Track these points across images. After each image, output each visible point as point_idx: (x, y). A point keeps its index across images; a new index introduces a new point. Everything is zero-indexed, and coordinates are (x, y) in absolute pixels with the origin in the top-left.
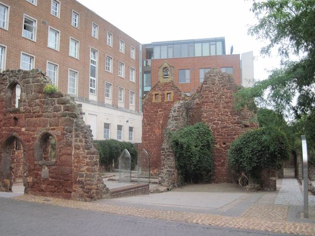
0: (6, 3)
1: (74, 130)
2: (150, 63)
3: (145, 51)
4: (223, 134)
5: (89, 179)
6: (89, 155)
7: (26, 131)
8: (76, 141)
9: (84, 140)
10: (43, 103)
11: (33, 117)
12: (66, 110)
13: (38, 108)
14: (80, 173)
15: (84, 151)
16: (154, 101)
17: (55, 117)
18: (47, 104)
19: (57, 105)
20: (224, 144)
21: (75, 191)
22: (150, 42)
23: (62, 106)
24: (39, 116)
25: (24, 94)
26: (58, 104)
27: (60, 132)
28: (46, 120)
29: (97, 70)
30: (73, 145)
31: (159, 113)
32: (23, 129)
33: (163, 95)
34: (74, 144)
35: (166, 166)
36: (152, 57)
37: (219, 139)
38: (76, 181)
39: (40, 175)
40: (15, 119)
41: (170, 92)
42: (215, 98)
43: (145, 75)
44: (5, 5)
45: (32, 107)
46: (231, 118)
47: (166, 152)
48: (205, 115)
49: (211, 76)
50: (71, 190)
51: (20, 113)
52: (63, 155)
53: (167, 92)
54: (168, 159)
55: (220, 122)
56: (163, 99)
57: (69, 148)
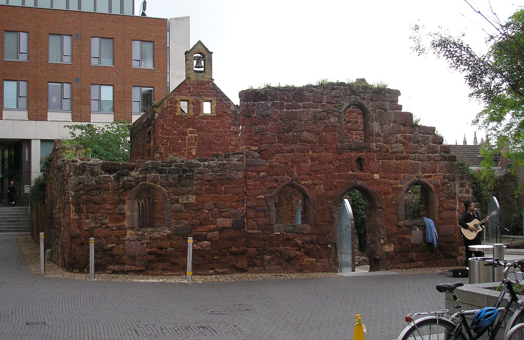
2: (95, 51)
8: (461, 192)
13: (400, 147)
28: (416, 163)
32: (376, 176)
40: (359, 160)
57: (452, 201)
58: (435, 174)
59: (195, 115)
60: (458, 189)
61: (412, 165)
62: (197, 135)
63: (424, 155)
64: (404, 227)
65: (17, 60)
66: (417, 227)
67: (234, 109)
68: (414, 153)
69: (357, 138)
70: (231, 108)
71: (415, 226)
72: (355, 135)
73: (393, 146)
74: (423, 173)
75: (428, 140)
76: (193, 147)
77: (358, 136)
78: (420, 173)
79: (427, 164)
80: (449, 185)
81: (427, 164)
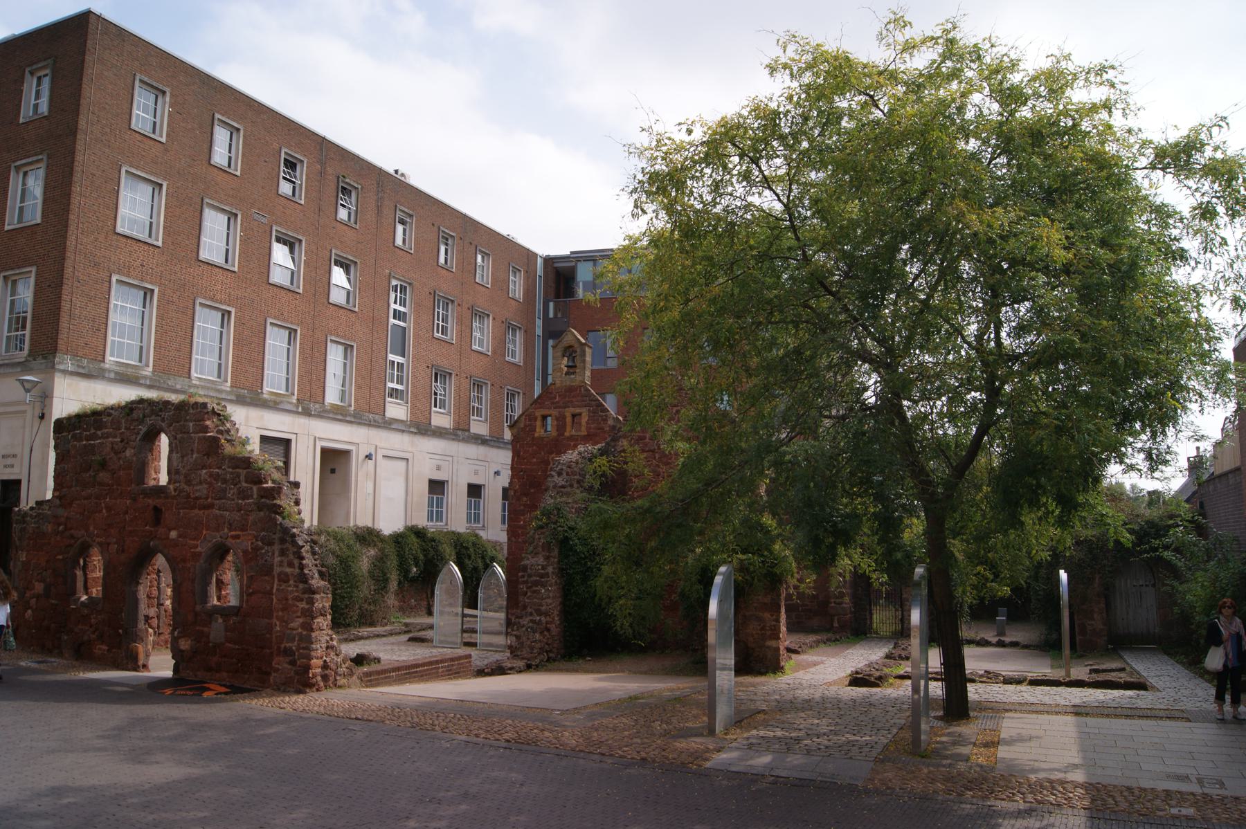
6: (306, 596)
9: (296, 562)
10: (216, 477)
11: (193, 508)
12: (262, 497)
13: (203, 490)
16: (539, 432)
17: (239, 510)
19: (245, 485)
21: (277, 670)
22: (566, 252)
23: (255, 488)
25: (174, 455)
26: (246, 482)
27: (250, 543)
30: (275, 573)
34: (277, 570)
35: (529, 610)
38: (279, 648)
39: (208, 637)
40: (157, 510)
44: (152, 178)
47: (530, 576)
51: (166, 498)
53: (572, 410)
54: (534, 592)
57: (266, 578)
59: (559, 435)
60: (277, 559)
65: (603, 367)
66: (219, 616)
68: (220, 499)
70: (609, 422)
74: (230, 529)
75: (239, 478)
78: (226, 530)
80: (263, 551)
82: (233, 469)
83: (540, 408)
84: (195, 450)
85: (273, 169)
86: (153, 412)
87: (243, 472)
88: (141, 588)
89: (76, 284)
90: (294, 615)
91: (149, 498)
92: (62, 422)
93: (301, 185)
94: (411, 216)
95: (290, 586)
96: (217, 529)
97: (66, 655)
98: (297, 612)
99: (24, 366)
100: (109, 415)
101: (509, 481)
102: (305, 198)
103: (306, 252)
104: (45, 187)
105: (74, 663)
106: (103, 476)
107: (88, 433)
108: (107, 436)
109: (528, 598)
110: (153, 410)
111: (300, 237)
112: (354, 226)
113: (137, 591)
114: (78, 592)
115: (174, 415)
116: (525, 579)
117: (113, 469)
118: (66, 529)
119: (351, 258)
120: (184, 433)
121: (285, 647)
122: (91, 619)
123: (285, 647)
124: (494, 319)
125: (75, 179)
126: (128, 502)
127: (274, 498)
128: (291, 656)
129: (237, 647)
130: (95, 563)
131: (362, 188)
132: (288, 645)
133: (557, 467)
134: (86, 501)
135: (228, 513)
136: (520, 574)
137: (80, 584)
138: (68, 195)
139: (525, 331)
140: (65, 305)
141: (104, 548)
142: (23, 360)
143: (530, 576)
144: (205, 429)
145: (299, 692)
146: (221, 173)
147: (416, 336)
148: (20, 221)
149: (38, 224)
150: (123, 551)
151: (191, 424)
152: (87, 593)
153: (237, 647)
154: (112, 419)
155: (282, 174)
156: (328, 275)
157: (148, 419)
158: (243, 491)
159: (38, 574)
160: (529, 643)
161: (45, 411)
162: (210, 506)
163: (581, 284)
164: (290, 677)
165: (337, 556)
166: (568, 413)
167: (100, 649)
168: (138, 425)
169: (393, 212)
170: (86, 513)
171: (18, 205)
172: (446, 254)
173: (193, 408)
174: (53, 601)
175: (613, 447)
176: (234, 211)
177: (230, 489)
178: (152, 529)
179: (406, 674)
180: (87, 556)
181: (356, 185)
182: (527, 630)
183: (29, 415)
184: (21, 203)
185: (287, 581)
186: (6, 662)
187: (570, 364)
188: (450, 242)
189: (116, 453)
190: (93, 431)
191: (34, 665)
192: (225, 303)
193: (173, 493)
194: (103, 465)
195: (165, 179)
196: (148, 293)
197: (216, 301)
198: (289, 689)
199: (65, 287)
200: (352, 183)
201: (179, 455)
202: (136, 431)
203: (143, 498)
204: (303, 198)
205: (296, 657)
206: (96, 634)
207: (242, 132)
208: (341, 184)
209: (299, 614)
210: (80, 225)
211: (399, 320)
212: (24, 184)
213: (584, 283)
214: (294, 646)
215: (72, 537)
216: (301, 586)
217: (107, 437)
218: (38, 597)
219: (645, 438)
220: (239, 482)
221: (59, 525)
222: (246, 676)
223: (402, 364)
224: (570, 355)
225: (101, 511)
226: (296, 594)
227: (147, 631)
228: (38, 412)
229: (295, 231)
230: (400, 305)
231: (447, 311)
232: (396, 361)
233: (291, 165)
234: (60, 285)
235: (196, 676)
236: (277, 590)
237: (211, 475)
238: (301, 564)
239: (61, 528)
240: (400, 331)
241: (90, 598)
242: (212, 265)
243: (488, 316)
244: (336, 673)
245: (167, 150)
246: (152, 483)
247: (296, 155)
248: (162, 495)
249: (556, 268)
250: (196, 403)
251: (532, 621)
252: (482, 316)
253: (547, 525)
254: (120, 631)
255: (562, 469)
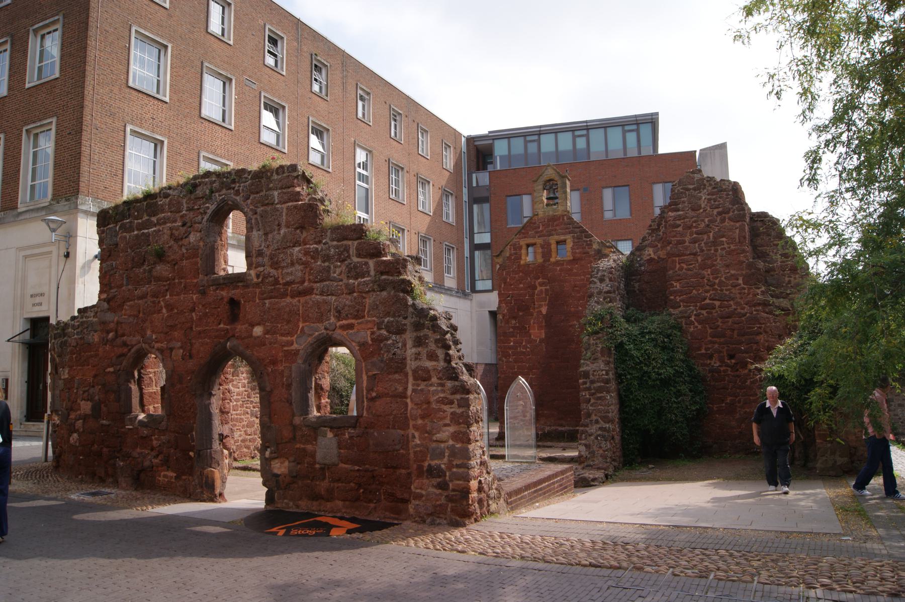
0: (162, 37)
1: (409, 327)
3: (473, 153)
4: (728, 333)
5: (459, 462)
6: (458, 396)
7: (265, 334)
8: (417, 357)
9: (440, 353)
10: (315, 255)
11: (284, 295)
12: (382, 273)
14: (434, 445)
15: (443, 385)
17: (351, 292)
18: (327, 258)
19: (355, 259)
20: (731, 357)
21: (419, 497)
22: (484, 132)
23: (371, 263)
24: (300, 294)
25: (255, 233)
26: (359, 256)
27: (369, 333)
29: (373, 195)
30: (408, 369)
31: (539, 288)
33: (546, 248)
34: (411, 365)
35: (594, 417)
36: (489, 166)
37: (716, 346)
38: (420, 468)
39: (313, 455)
40: (234, 303)
41: (562, 238)
42: (703, 245)
43: (475, 207)
45: (283, 268)
46: (746, 291)
47: (592, 382)
48: (677, 286)
49: (688, 190)
50: (406, 496)
51: (247, 286)
52: (379, 396)
53: (556, 238)
54: (600, 398)
55: (717, 303)
56: (547, 254)
57: (397, 376)
58: (360, 321)
59: (544, 261)
60: (410, 351)
61: (318, 304)
62: (548, 287)
63: (341, 283)
64: (304, 429)
67: (598, 247)
68: (321, 281)
69: (681, 269)
70: (594, 247)
71: (325, 427)
72: (679, 263)
73: (285, 271)
74: (339, 318)
75: (348, 252)
76: (543, 303)
77: (682, 265)
78: (333, 320)
79: (346, 300)
80: (390, 342)
81: (346, 300)
82: (338, 241)
83: (525, 237)
84: (283, 224)
85: (260, 43)
86: (224, 186)
87: (353, 245)
88: (214, 400)
89: (94, 131)
90: (441, 423)
91: (223, 289)
92: (108, 212)
93: (283, 58)
94: (368, 94)
95: (431, 385)
96: (320, 320)
97: (124, 485)
98: (445, 418)
99: (48, 209)
100: (166, 196)
101: (497, 306)
102: (287, 69)
103: (289, 117)
104: (62, 44)
105: (134, 493)
106: (162, 269)
107: (140, 221)
108: (164, 221)
109: (592, 405)
110: (223, 183)
111: (283, 104)
112: (325, 97)
113: (210, 404)
114: (133, 410)
115: (252, 184)
116: (588, 385)
117: (173, 260)
118: (116, 336)
119: (325, 126)
120: (267, 204)
121: (429, 465)
122: (151, 440)
123: (429, 465)
124: (433, 185)
125: (90, 33)
126: (194, 297)
127: (400, 273)
128: (440, 477)
129: (357, 468)
130: (151, 375)
131: (331, 66)
132: (433, 463)
133: (597, 273)
134: (140, 301)
135: (334, 298)
136: (581, 381)
137: (135, 401)
138: (84, 48)
139: (456, 197)
140: (85, 150)
141: (165, 354)
142: (47, 204)
143: (592, 382)
144: (297, 196)
145: (457, 525)
146: (217, 41)
147: (377, 196)
148: (39, 78)
149: (57, 79)
150: (191, 357)
151: (276, 193)
152: (143, 411)
153: (357, 468)
154: (171, 200)
155: (267, 48)
156: (306, 139)
157: (217, 194)
158: (355, 267)
159: (84, 392)
160: (601, 452)
161: (69, 250)
162: (309, 292)
163: (498, 158)
164: (440, 505)
165: (348, 379)
166: (553, 240)
167: (165, 476)
168: (204, 203)
169: (355, 89)
170: (141, 315)
171: (30, 183)
172: (395, 128)
173: (278, 174)
174: (104, 422)
175: (639, 256)
176: (229, 76)
177: (336, 267)
178: (228, 327)
179: (535, 492)
180: (142, 368)
181: (325, 63)
182: (596, 438)
183: (55, 254)
184: (32, 181)
185: (427, 379)
186: (53, 495)
187: (552, 196)
188: (398, 118)
189: (177, 240)
190: (146, 218)
191: (89, 499)
192: (224, 157)
193: (255, 280)
194: (160, 256)
195: (170, 41)
196: (158, 144)
197: (217, 155)
198: (438, 521)
199: (84, 133)
200: (323, 61)
201: (261, 233)
202: (201, 211)
203: (215, 290)
204: (285, 70)
205: (447, 478)
206: (160, 458)
207: (233, 6)
208: (314, 62)
209: (447, 421)
210: (96, 77)
211: (363, 182)
212: (42, 46)
213: (501, 157)
214: (443, 463)
215: (125, 344)
216: (449, 384)
217: (165, 223)
218: (85, 418)
219: (684, 242)
220: (349, 257)
221: (108, 332)
222: (372, 505)
223: (367, 220)
224: (551, 188)
225: (159, 311)
226: (442, 395)
227: (223, 452)
228: (63, 251)
229: (280, 98)
230: (363, 169)
231: (398, 177)
232: (362, 217)
233: (273, 41)
234: (79, 131)
235: (298, 507)
236: (414, 391)
237: (306, 253)
238: (447, 355)
239: (111, 335)
240: (364, 191)
241: (149, 416)
242: (213, 122)
243: (429, 182)
244: (488, 496)
245: (170, 16)
246: (222, 273)
247: (278, 32)
248: (240, 284)
249: (475, 146)
250: (282, 167)
251: (601, 429)
252: (425, 182)
253: (602, 329)
254: (191, 454)
255: (604, 276)
